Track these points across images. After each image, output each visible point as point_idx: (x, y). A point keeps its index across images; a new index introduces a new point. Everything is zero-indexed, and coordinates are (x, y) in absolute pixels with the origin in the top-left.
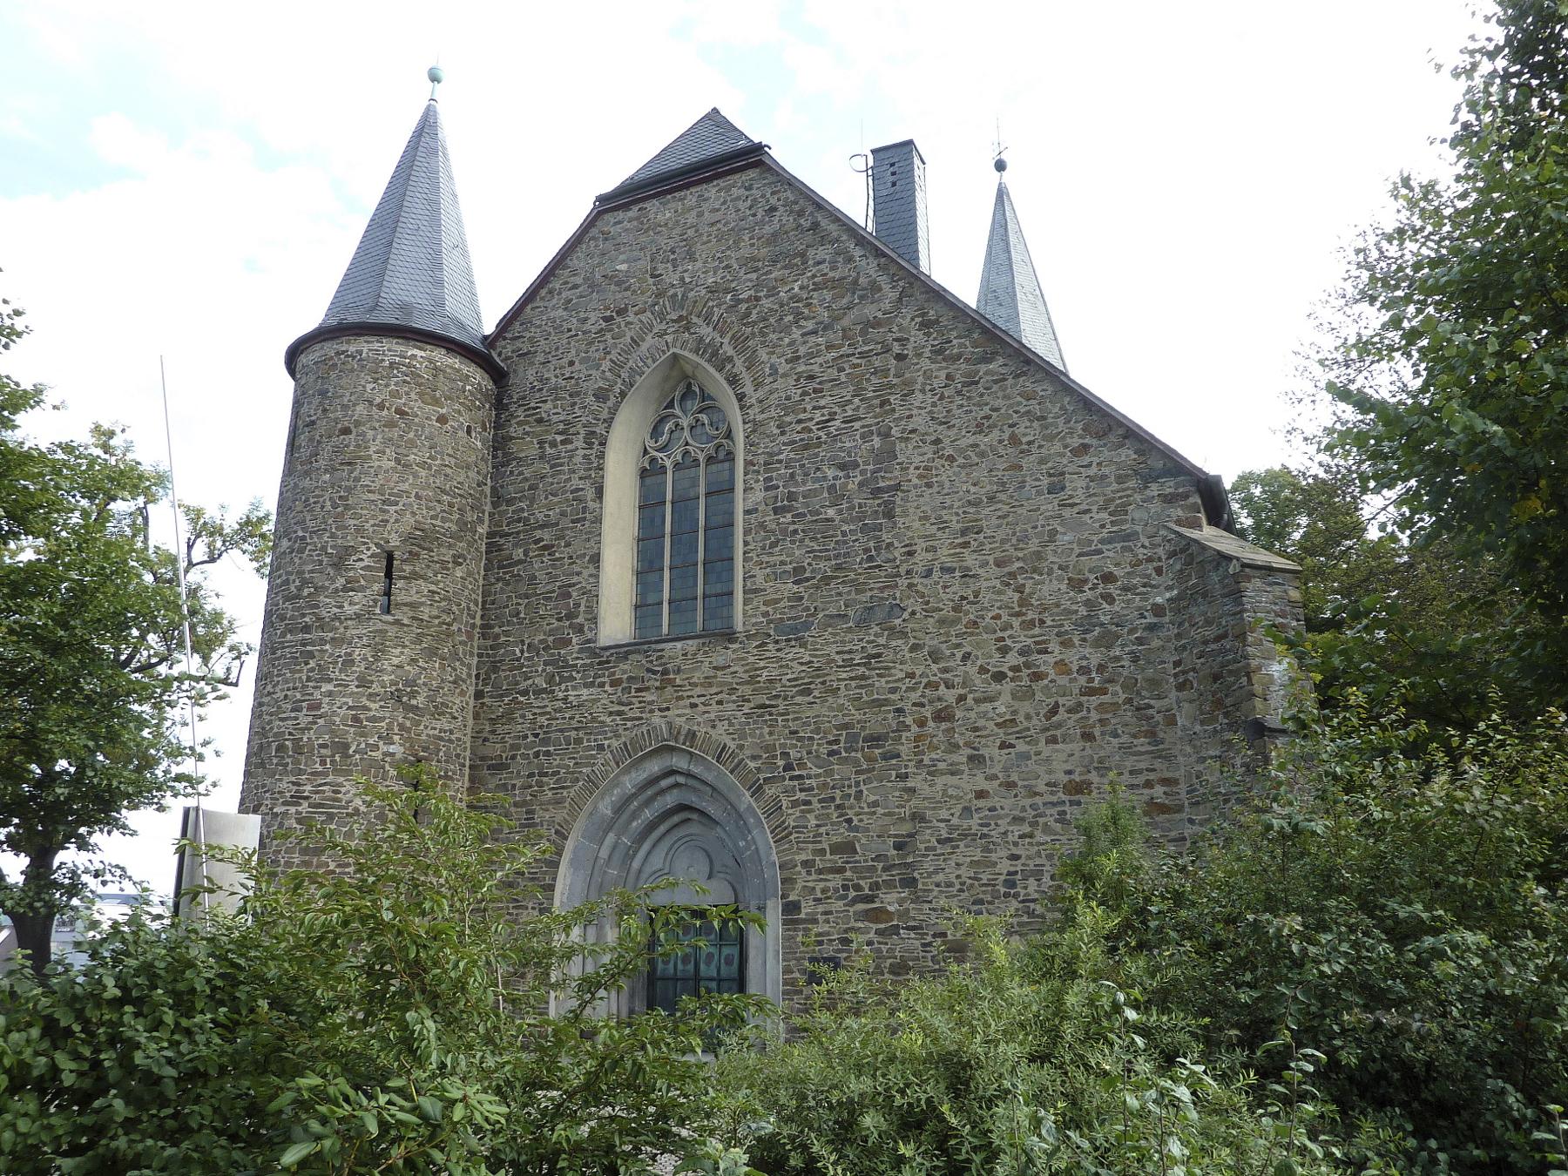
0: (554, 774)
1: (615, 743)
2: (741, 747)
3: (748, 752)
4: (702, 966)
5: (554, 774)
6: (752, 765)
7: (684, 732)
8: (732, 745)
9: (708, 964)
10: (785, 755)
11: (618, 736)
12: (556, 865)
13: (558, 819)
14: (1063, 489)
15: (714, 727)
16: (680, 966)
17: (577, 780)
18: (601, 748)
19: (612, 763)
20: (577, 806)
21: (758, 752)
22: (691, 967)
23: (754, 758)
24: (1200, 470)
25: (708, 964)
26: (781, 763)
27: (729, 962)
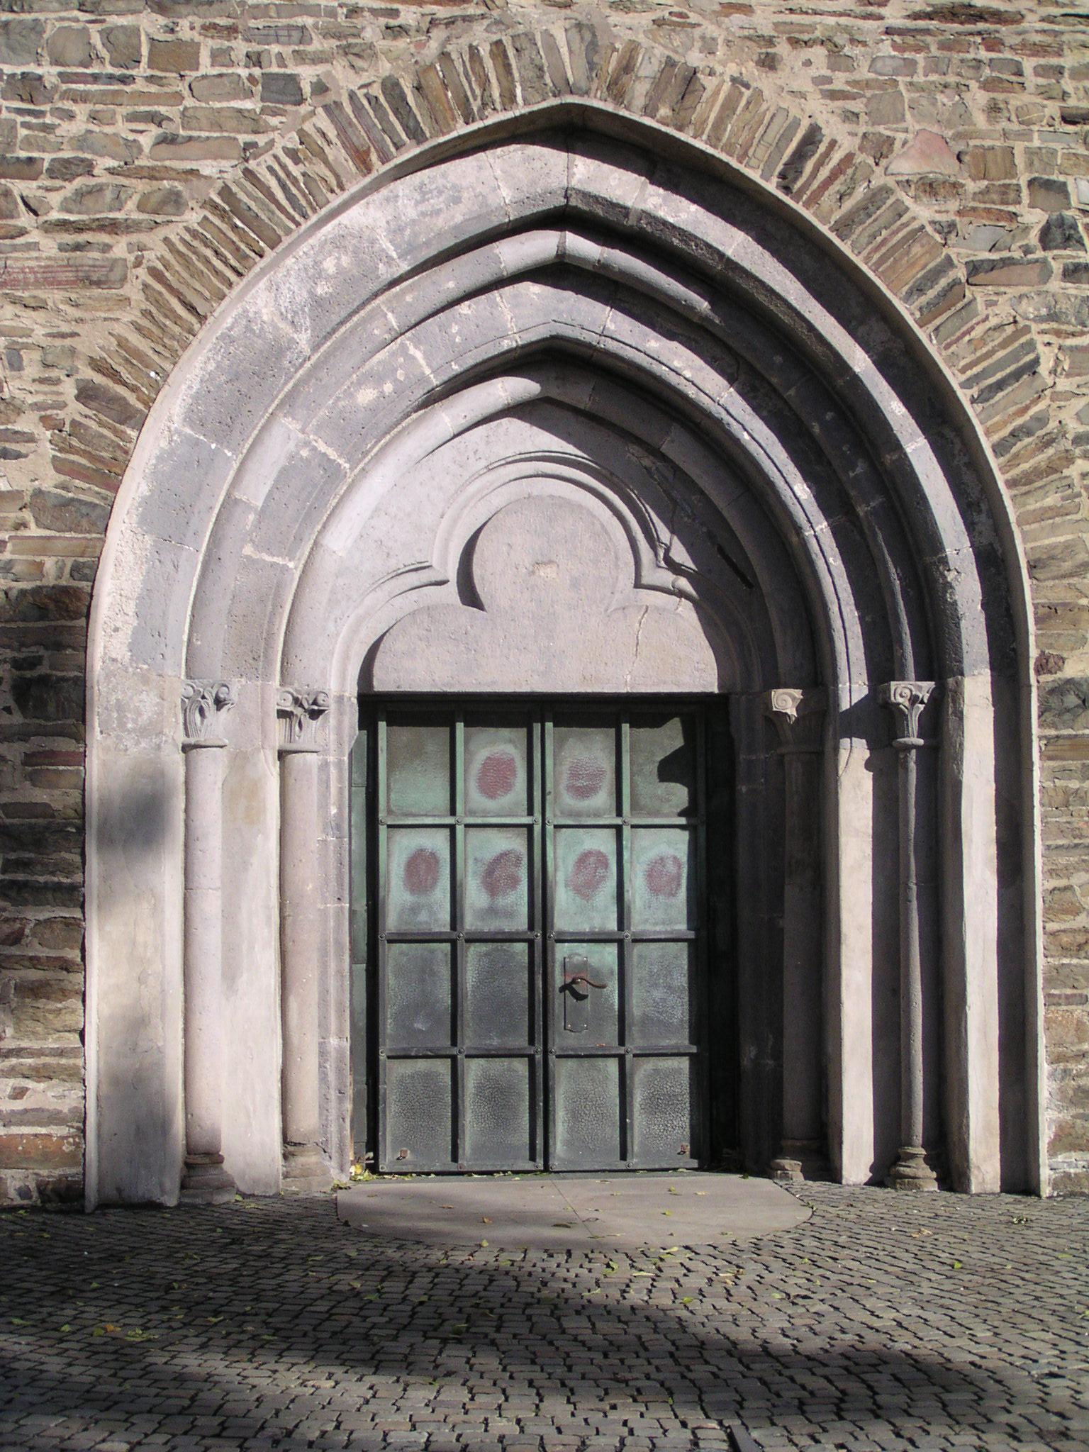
0: (64, 170)
1: (345, 79)
2: (881, 149)
3: (904, 166)
4: (563, 898)
5: (64, 170)
6: (923, 212)
7: (648, 68)
8: (842, 137)
9: (585, 889)
10: (1049, 188)
11: (355, 52)
12: (100, 519)
13: (94, 341)
14: (608, 88)
15: (769, 63)
16: (475, 896)
17: (174, 201)
18: (283, 90)
19: (336, 153)
20: (179, 307)
21: (946, 168)
22: (518, 899)
23: (930, 188)
24: (471, 238)
25: (585, 889)
26: (1035, 218)
27: (493, 879)
